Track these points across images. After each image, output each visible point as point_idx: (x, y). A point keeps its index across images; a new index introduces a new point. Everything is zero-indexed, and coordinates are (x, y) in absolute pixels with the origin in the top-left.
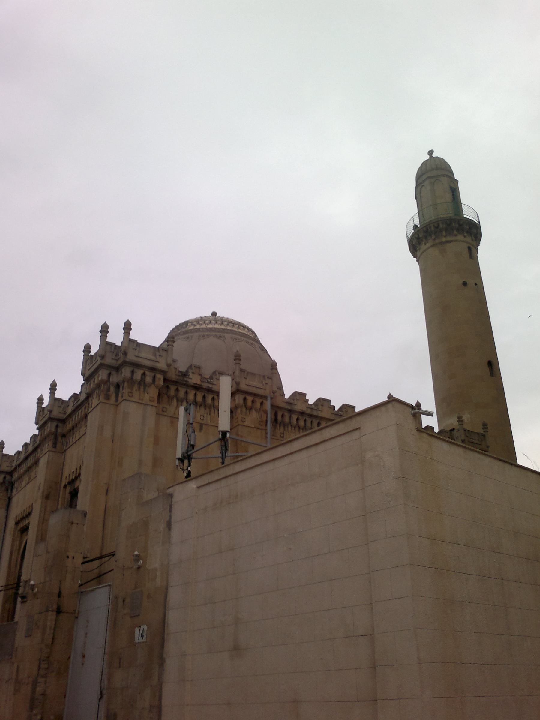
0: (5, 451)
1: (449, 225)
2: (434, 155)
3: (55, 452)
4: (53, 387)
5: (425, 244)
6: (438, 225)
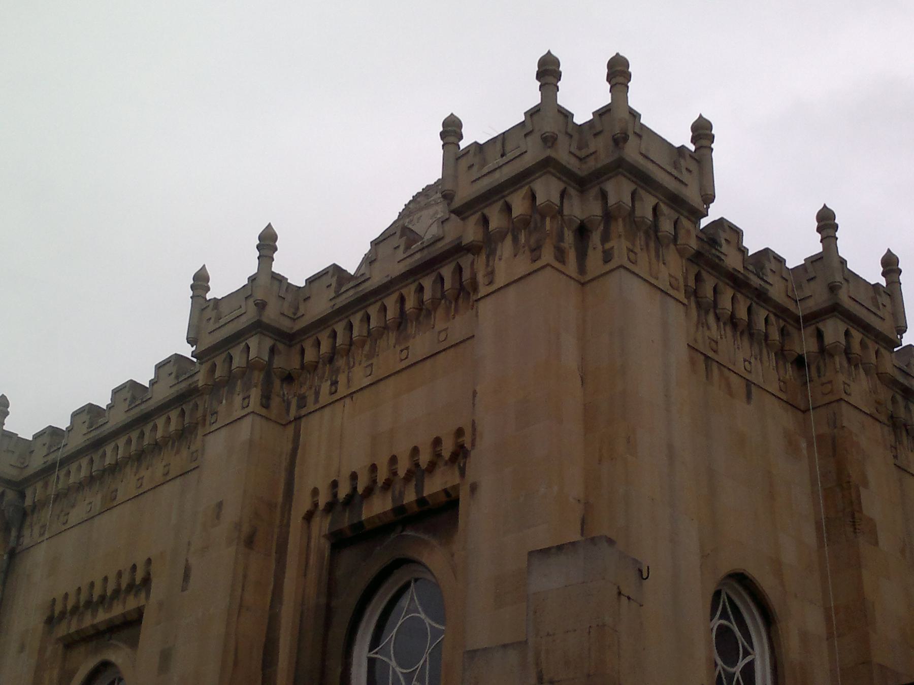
0: (10, 425)
3: (267, 418)
4: (267, 243)
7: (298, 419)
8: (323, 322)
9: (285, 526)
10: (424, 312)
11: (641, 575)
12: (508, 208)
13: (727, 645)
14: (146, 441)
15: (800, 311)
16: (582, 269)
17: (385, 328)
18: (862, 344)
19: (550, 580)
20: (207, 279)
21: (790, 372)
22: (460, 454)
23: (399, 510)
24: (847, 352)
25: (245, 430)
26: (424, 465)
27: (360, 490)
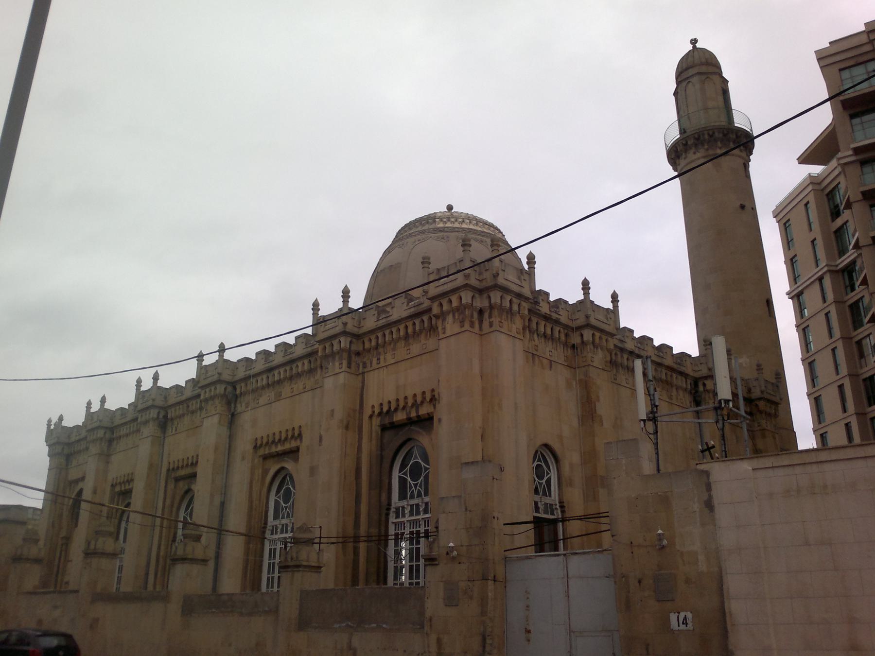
1: (725, 135)
2: (698, 45)
5: (695, 153)
6: (714, 133)
7: (363, 373)
8: (372, 332)
9: (361, 420)
10: (416, 335)
11: (502, 470)
12: (450, 301)
13: (539, 472)
14: (294, 372)
15: (574, 325)
16: (481, 329)
17: (399, 338)
18: (600, 338)
19: (469, 474)
20: (349, 292)
21: (569, 352)
22: (433, 400)
23: (409, 419)
24: (593, 342)
25: (342, 378)
26: (419, 402)
27: (392, 409)
